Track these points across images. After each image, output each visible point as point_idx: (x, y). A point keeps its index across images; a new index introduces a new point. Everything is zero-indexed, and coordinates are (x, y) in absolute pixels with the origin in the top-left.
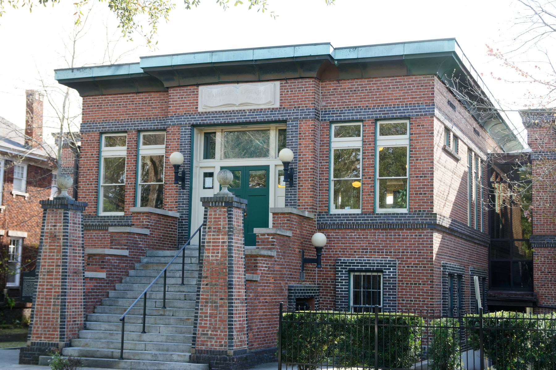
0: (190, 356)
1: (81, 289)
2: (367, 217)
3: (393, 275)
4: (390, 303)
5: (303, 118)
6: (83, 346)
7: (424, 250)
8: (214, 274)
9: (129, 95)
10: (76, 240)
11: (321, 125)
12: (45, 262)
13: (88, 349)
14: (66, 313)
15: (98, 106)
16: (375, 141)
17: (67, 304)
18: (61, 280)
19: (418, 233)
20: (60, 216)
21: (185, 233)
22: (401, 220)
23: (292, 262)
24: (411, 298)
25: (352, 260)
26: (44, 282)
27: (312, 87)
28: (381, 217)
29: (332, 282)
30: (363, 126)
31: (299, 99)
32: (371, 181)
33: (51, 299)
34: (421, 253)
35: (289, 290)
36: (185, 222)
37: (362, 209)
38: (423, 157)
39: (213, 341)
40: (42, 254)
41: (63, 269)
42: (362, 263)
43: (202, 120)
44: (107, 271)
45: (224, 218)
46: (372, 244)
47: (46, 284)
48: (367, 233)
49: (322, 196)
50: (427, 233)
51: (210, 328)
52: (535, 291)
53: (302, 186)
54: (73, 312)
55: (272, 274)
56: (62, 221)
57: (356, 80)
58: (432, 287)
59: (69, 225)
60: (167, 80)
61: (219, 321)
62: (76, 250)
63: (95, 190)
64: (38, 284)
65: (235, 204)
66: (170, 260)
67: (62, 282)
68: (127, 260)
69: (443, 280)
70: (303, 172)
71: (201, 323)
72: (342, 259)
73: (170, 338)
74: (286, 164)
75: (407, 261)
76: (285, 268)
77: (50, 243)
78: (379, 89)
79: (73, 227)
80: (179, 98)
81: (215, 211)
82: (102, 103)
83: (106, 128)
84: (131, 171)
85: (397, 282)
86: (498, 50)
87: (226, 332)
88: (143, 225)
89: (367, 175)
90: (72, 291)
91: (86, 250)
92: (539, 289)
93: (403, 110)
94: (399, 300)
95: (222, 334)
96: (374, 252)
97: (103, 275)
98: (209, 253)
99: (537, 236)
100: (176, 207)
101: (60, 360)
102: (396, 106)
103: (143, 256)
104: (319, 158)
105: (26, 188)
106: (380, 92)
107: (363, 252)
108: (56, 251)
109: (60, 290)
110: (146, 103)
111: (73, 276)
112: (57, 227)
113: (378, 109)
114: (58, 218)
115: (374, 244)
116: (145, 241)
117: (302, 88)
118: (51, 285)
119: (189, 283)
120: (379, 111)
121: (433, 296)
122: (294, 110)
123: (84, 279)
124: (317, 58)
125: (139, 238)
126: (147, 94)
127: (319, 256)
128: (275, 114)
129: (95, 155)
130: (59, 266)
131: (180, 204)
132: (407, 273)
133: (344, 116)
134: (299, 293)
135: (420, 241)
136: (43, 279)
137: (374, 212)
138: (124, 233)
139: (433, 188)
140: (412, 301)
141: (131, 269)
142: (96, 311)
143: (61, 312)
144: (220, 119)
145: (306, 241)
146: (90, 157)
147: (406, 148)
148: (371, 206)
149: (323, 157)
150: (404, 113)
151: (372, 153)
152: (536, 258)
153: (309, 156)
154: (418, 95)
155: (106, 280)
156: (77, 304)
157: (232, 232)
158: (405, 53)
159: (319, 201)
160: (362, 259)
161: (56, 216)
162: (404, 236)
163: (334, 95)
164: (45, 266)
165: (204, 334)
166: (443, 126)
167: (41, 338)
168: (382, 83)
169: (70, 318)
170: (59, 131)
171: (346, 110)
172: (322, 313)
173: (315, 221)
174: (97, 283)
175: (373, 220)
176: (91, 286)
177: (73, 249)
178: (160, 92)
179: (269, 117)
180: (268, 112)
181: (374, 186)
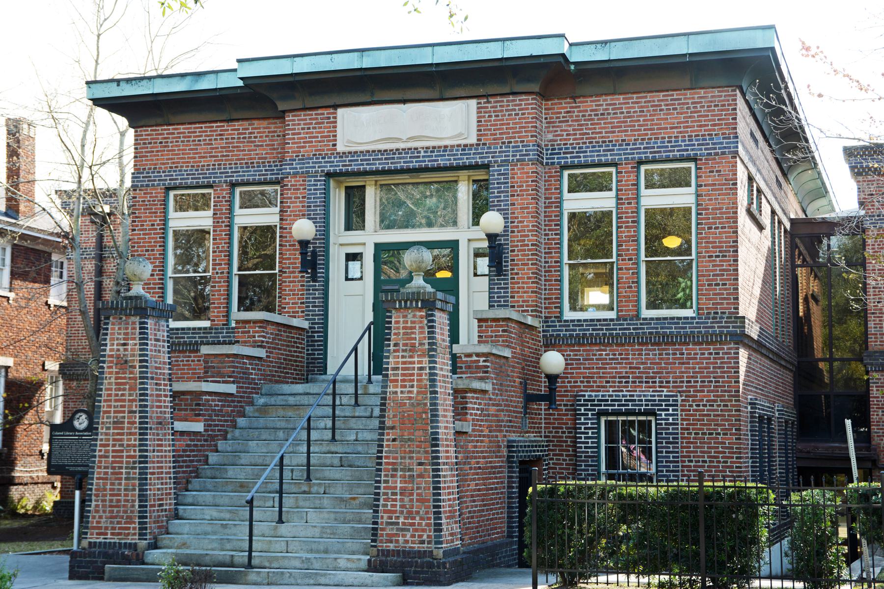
0: (369, 561)
1: (169, 451)
3: (673, 419)
4: (669, 467)
5: (518, 160)
6: (178, 548)
7: (724, 377)
8: (407, 422)
9: (215, 125)
10: (160, 368)
11: (546, 173)
13: (188, 551)
14: (148, 492)
15: (161, 143)
16: (637, 197)
17: (149, 476)
18: (138, 437)
19: (714, 349)
20: (134, 328)
21: (318, 354)
23: (511, 401)
24: (704, 457)
25: (603, 396)
27: (532, 109)
28: (650, 324)
29: (569, 433)
30: (618, 173)
31: (511, 128)
32: (633, 264)
33: (121, 468)
34: (719, 382)
35: (508, 447)
36: (318, 336)
37: (618, 311)
38: (720, 223)
39: (408, 535)
40: (103, 392)
41: (140, 417)
42: (621, 401)
43: (343, 166)
44: (206, 420)
45: (421, 328)
48: (628, 350)
49: (550, 290)
50: (728, 349)
51: (402, 512)
52: (873, 443)
53: (517, 274)
54: (159, 489)
55: (486, 421)
56: (137, 336)
57: (604, 97)
58: (740, 439)
59: (149, 342)
60: (285, 98)
61: (418, 500)
62: (160, 385)
63: (159, 284)
64: (98, 443)
65: (439, 304)
66: (305, 400)
67: (140, 440)
68: (233, 401)
69: (751, 426)
71: (386, 506)
73: (328, 531)
75: (696, 396)
76: (503, 410)
77: (117, 373)
79: (155, 346)
80: (303, 129)
81: (405, 316)
82: (168, 138)
84: (220, 252)
85: (680, 431)
86: (818, 48)
87: (429, 519)
88: (255, 342)
89: (626, 255)
90: (155, 454)
93: (685, 145)
94: (684, 462)
95: (424, 523)
96: (639, 382)
97: (198, 427)
98: (396, 387)
99: (876, 352)
100: (303, 312)
101: (178, 572)
102: (673, 139)
103: (257, 393)
104: (543, 227)
105: (11, 283)
106: (646, 116)
107: (621, 382)
108: (127, 387)
109: (138, 454)
111: (157, 429)
112: (129, 347)
113: (642, 144)
114: (129, 331)
115: (639, 368)
116: (259, 370)
117: (515, 110)
118: (122, 445)
119: (343, 439)
120: (645, 148)
121: (740, 453)
122: (501, 147)
123: (173, 435)
124: (542, 60)
125: (250, 364)
126: (246, 123)
127: (552, 390)
128: (470, 154)
129: (158, 225)
130: (135, 412)
131: (308, 307)
133: (584, 157)
134: (523, 452)
135: (717, 363)
136: (106, 434)
137: (637, 317)
138: (228, 356)
139: (737, 275)
140: (705, 462)
141: (240, 416)
142: (190, 487)
143: (140, 490)
144: (375, 164)
145: (529, 366)
146: (150, 230)
147: (690, 208)
149: (551, 225)
150: (687, 150)
151: (633, 217)
152: (875, 389)
153: (529, 223)
154: (710, 120)
155: (204, 436)
156: (164, 475)
157: (435, 350)
158: (690, 52)
159: (545, 299)
160: (620, 394)
161: (127, 329)
162: (690, 354)
163: (568, 121)
164: (109, 412)
166: (746, 173)
167: (106, 534)
168: (649, 102)
169: (154, 500)
170: (74, 186)
171: (588, 147)
172: (566, 484)
173: (539, 332)
174: (191, 440)
175: (637, 329)
176: (181, 445)
177: (156, 384)
178: (269, 118)
179: (459, 159)
180: (457, 150)
181: (637, 273)
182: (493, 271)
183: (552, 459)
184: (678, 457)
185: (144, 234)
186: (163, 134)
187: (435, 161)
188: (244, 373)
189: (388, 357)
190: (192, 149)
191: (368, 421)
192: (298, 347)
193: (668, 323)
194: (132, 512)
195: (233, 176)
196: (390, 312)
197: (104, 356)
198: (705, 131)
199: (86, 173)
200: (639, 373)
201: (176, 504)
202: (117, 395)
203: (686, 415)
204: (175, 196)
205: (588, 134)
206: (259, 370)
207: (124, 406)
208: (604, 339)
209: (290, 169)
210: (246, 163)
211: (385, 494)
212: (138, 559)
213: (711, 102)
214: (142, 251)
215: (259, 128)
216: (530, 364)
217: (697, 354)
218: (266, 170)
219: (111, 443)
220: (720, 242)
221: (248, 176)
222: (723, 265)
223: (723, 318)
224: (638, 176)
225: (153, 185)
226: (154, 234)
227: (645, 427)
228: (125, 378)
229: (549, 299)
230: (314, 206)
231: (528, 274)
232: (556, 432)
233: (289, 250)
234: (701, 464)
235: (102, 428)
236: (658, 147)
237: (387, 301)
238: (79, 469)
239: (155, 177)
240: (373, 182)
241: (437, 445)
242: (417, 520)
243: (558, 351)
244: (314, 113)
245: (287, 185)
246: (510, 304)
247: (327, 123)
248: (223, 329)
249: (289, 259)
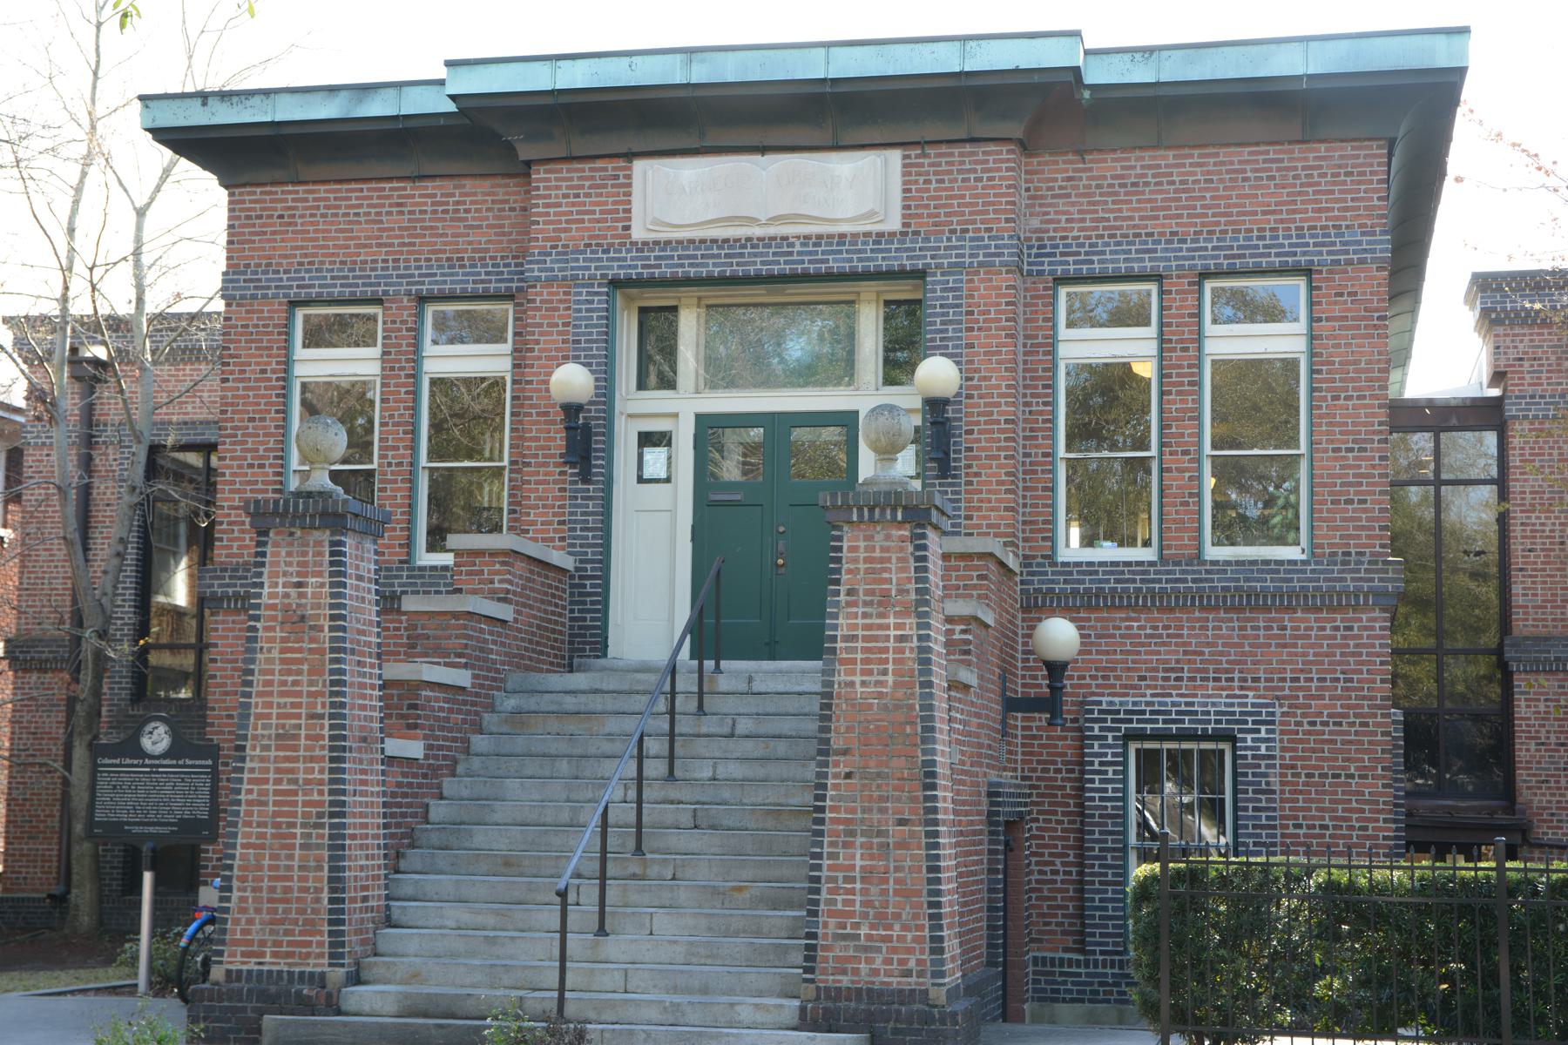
0: (803, 1009)
2: (1183, 572)
3: (1268, 749)
5: (981, 264)
9: (388, 186)
11: (1026, 290)
12: (269, 705)
13: (426, 990)
14: (347, 874)
15: (281, 217)
16: (1199, 338)
18: (327, 765)
21: (592, 619)
22: (1291, 580)
24: (1323, 818)
25: (1135, 704)
27: (1008, 169)
28: (1225, 571)
29: (1068, 771)
32: (1190, 461)
33: (294, 825)
34: (1351, 680)
36: (592, 586)
37: (1161, 548)
38: (1354, 389)
39: (879, 959)
41: (332, 727)
42: (1170, 712)
43: (644, 267)
44: (426, 737)
46: (1195, 653)
47: (271, 776)
48: (1180, 620)
50: (1369, 620)
51: (865, 916)
52: (1520, 800)
53: (977, 474)
54: (362, 868)
56: (326, 569)
57: (1138, 153)
61: (896, 893)
63: (275, 482)
64: (246, 776)
67: (332, 771)
68: (465, 703)
72: (1104, 699)
73: (702, 951)
74: (935, 406)
77: (284, 640)
79: (357, 588)
80: (566, 196)
83: (313, 286)
88: (494, 591)
90: (358, 798)
91: (385, 665)
92: (1533, 793)
93: (1291, 245)
94: (1287, 827)
95: (909, 935)
98: (853, 673)
99: (1527, 638)
100: (562, 539)
103: (499, 689)
106: (1217, 189)
109: (327, 798)
111: (360, 750)
112: (309, 590)
113: (1210, 240)
114: (310, 558)
115: (1202, 653)
117: (975, 171)
118: (296, 781)
119: (688, 775)
120: (1214, 248)
122: (949, 239)
124: (1036, 78)
127: (1056, 690)
128: (889, 251)
129: (274, 372)
130: (321, 717)
131: (574, 529)
132: (1308, 741)
135: (1348, 646)
136: (262, 759)
137: (1198, 557)
138: (456, 615)
140: (1325, 827)
142: (403, 865)
143: (331, 869)
144: (707, 265)
146: (257, 380)
150: (1295, 254)
152: (1523, 703)
153: (999, 381)
155: (421, 766)
157: (927, 603)
158: (1310, 72)
159: (1024, 523)
160: (1168, 700)
161: (305, 554)
162: (1298, 628)
163: (1069, 195)
164: (269, 716)
165: (845, 937)
167: (263, 955)
168: (1223, 163)
171: (1108, 245)
172: (1288, 864)
174: (404, 775)
175: (1201, 580)
179: (868, 259)
180: (865, 243)
182: (931, 469)
183: (1037, 820)
184: (1274, 818)
185: (245, 389)
186: (286, 200)
187: (822, 261)
188: (482, 650)
191: (731, 743)
192: (556, 605)
193: (1258, 571)
194: (314, 911)
195: (423, 283)
196: (839, 528)
197: (258, 606)
199: (79, 286)
200: (1202, 662)
201: (388, 898)
203: (1289, 741)
204: (307, 318)
205: (1108, 220)
207: (299, 705)
208: (1137, 598)
209: (540, 270)
210: (448, 259)
211: (830, 879)
212: (329, 1005)
213: (1340, 166)
214: (242, 420)
215: (475, 194)
216: (1013, 642)
217: (1311, 629)
218: (487, 273)
219: (271, 776)
220: (1354, 424)
221: (452, 282)
222: (1359, 467)
223: (1362, 563)
224: (1200, 299)
225: (265, 296)
226: (266, 388)
228: (300, 650)
229: (1031, 522)
230: (587, 341)
231: (999, 475)
232: (1044, 770)
234: (1317, 831)
235: (254, 748)
237: (834, 506)
238: (152, 830)
239: (268, 280)
240: (695, 301)
241: (934, 787)
242: (896, 932)
243: (1072, 620)
245: (534, 301)
247: (613, 186)
248: (402, 569)
249: (537, 439)
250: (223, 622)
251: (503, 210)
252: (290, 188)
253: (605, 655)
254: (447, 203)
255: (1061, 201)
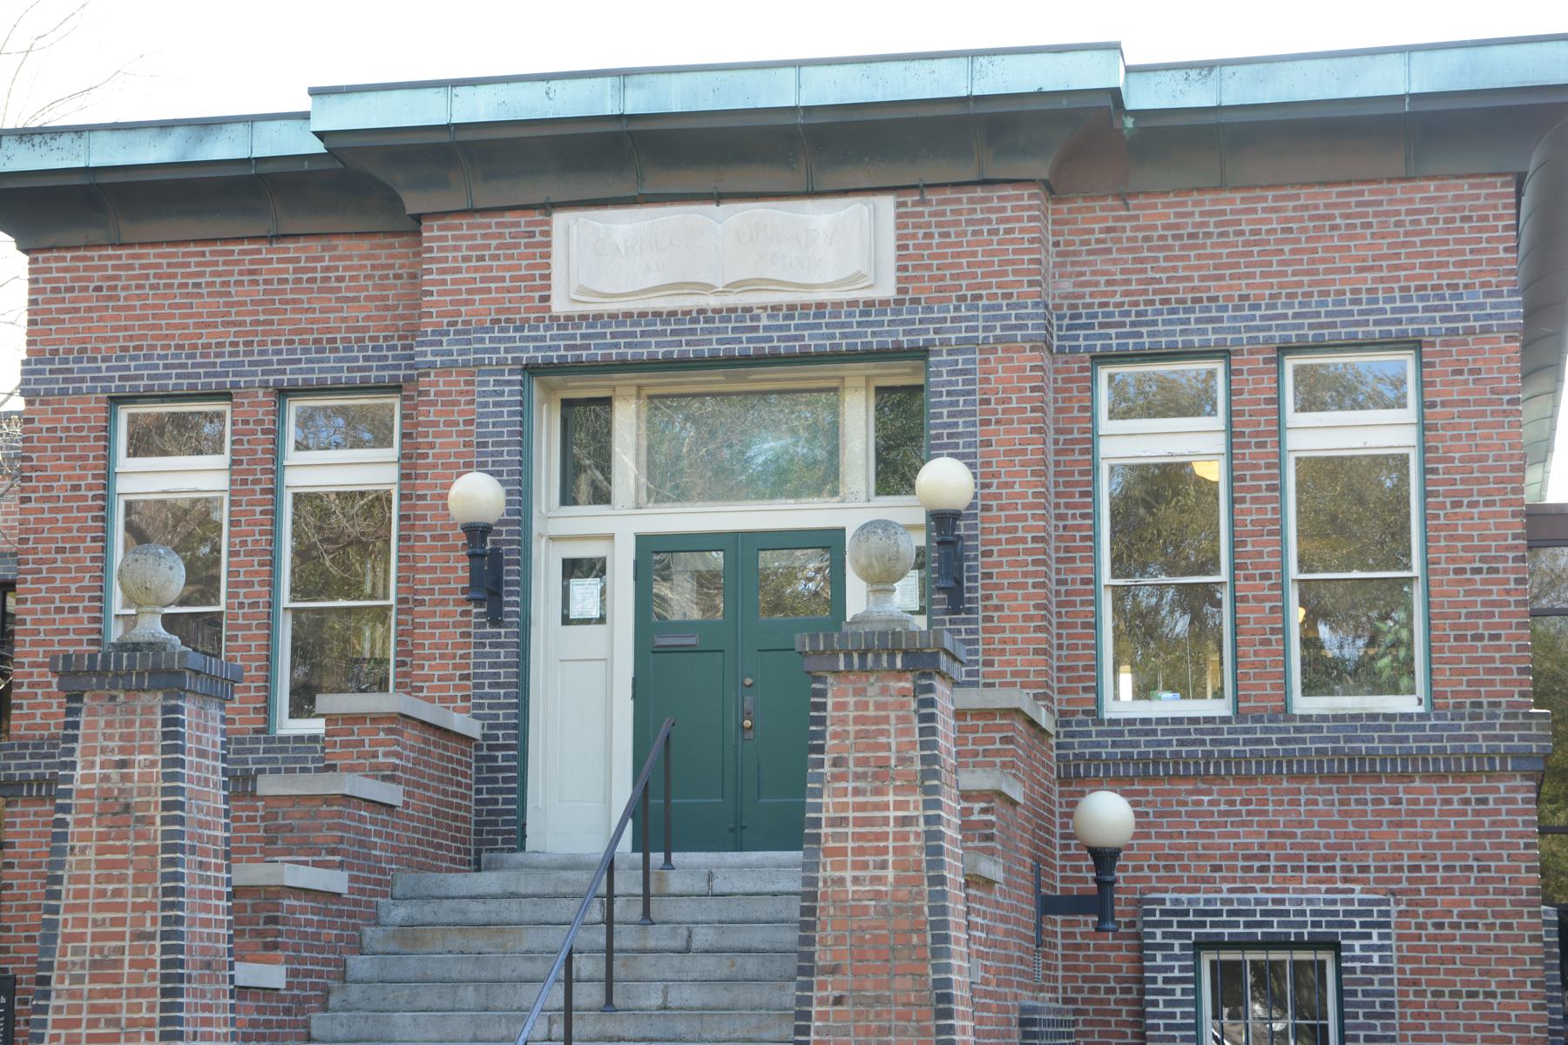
2: (1266, 730)
3: (1382, 959)
5: (998, 340)
7: (1500, 858)
8: (871, 955)
9: (236, 248)
11: (1056, 371)
12: (83, 922)
18: (158, 1000)
21: (505, 802)
22: (1406, 739)
25: (1207, 902)
26: (79, 1009)
27: (1031, 219)
28: (1320, 729)
29: (1124, 991)
32: (1271, 587)
34: (1488, 869)
36: (505, 758)
37: (1237, 699)
38: (1480, 493)
41: (165, 950)
42: (1253, 913)
43: (567, 348)
44: (288, 960)
45: (900, 719)
48: (1264, 792)
49: (1070, 647)
50: (1509, 790)
53: (998, 608)
56: (158, 742)
57: (1196, 196)
59: (187, 758)
63: (91, 631)
64: (50, 1017)
66: (512, 911)
68: (340, 913)
70: (1001, 553)
72: (1168, 896)
75: (1435, 903)
77: (102, 837)
78: (1290, 230)
79: (199, 767)
80: (466, 259)
82: (117, 278)
93: (1394, 310)
96: (1294, 869)
98: (842, 866)
100: (466, 698)
103: (384, 895)
106: (1298, 241)
110: (312, 280)
111: (202, 979)
112: (136, 771)
113: (1291, 306)
114: (136, 729)
115: (1293, 835)
117: (989, 221)
120: (1296, 316)
122: (957, 309)
125: (374, 822)
127: (1105, 885)
128: (881, 323)
129: (89, 487)
130: (151, 936)
133: (1150, 334)
135: (1482, 824)
136: (72, 994)
137: (1285, 711)
138: (328, 799)
146: (67, 499)
148: (1273, 687)
149: (1072, 495)
150: (1399, 322)
151: (1271, 477)
153: (1024, 488)
154: (1451, 253)
155: (282, 999)
158: (1414, 90)
159: (1060, 669)
161: (129, 724)
163: (1109, 251)
164: (81, 937)
168: (1305, 208)
171: (1160, 312)
174: (260, 1010)
179: (854, 335)
180: (850, 315)
185: (51, 510)
186: (105, 268)
187: (795, 338)
188: (362, 844)
189: (818, 793)
190: (178, 306)
192: (459, 784)
193: (1363, 728)
195: (283, 372)
198: (1440, 276)
200: (1293, 846)
202: (101, 893)
205: (1159, 281)
206: (389, 836)
207: (122, 922)
208: (1207, 764)
209: (435, 354)
210: (316, 341)
213: (1455, 210)
215: (350, 258)
216: (1049, 823)
217: (1433, 802)
219: (84, 1016)
220: (1482, 538)
221: (321, 370)
222: (1490, 592)
223: (1497, 716)
224: (1279, 381)
227: (1308, 976)
229: (1069, 669)
230: (495, 444)
231: (1026, 608)
233: (433, 549)
235: (61, 980)
236: (1328, 314)
237: (815, 652)
239: (81, 370)
240: (634, 390)
241: (949, 1014)
243: (1124, 794)
244: (494, 221)
245: (427, 393)
246: (982, 681)
247: (527, 246)
248: (257, 741)
250: (23, 814)
251: (386, 277)
252: (110, 252)
253: (522, 848)
254: (314, 270)
255: (1099, 258)
